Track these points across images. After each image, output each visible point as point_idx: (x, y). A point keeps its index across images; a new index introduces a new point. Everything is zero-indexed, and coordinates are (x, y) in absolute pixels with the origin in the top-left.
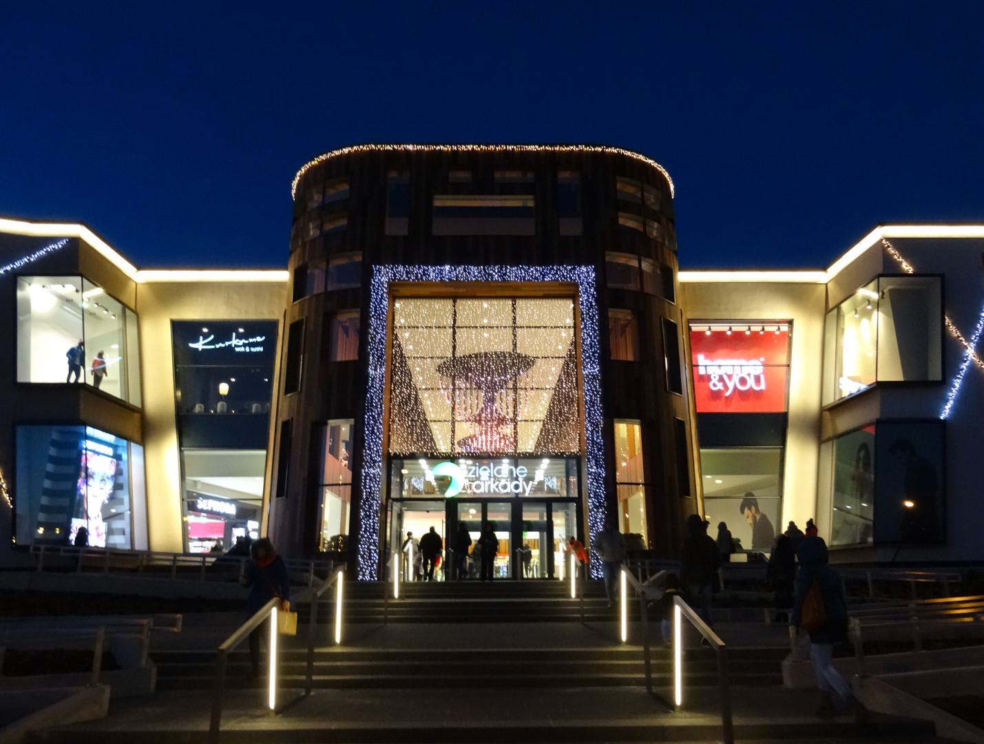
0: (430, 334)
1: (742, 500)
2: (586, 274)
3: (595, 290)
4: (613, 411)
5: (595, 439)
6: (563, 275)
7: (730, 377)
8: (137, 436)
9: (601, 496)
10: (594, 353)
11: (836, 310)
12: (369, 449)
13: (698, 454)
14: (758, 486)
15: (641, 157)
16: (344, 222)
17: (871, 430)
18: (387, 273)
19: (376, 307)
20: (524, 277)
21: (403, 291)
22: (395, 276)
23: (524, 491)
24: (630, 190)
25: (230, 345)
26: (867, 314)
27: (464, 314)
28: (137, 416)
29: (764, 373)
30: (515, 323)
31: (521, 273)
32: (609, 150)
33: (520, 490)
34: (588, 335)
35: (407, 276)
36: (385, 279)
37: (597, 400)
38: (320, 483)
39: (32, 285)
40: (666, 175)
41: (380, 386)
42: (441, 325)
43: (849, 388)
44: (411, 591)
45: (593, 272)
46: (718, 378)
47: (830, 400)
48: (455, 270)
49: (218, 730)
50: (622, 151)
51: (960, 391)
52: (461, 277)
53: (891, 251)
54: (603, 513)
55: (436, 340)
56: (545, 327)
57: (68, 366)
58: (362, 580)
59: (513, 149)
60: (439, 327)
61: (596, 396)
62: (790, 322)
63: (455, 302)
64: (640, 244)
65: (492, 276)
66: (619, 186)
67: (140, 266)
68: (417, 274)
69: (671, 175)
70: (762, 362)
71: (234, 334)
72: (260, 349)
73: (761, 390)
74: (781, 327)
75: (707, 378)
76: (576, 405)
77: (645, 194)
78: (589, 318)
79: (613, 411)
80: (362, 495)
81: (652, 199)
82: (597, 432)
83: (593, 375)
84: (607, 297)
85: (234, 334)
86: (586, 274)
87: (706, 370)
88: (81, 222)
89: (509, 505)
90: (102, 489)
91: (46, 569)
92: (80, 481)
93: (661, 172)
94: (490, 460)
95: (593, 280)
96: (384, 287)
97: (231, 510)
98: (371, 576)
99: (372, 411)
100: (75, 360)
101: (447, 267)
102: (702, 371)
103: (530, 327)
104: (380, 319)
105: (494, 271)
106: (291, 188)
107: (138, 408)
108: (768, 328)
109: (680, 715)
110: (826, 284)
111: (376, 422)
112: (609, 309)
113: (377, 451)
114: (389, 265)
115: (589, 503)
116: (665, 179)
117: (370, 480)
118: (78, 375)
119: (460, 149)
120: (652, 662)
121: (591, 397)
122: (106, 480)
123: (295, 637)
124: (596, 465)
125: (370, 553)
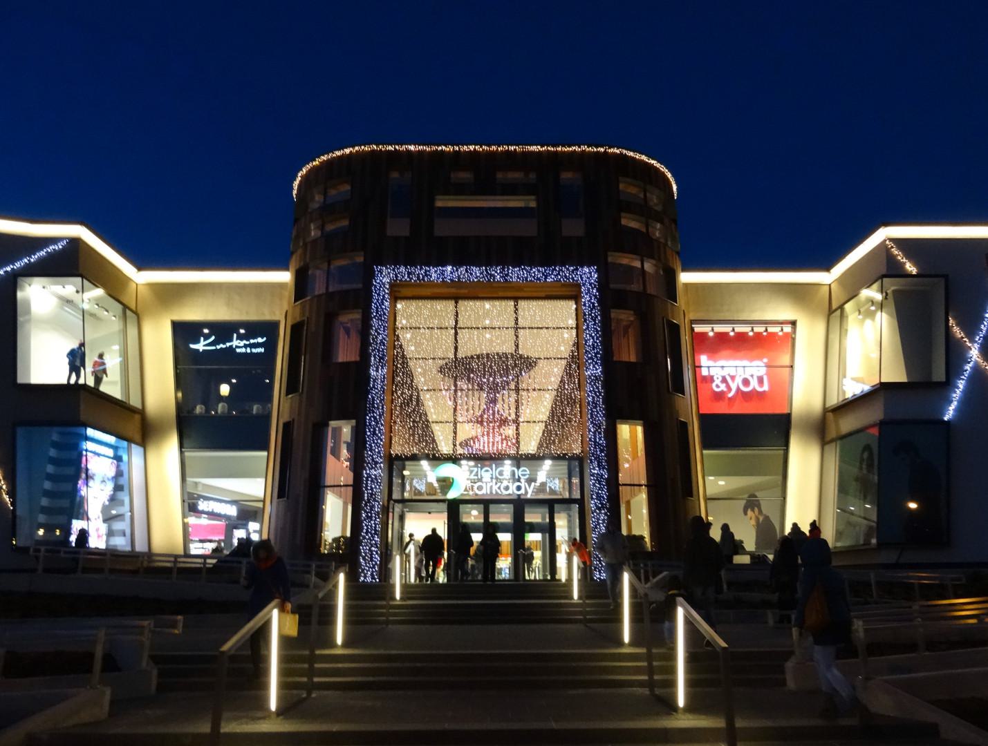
0: (431, 335)
1: (745, 501)
2: (588, 275)
3: (597, 291)
4: (616, 412)
5: (598, 440)
6: (566, 276)
7: (733, 378)
8: (138, 437)
9: (603, 497)
10: (596, 354)
11: (839, 311)
12: (371, 450)
13: (701, 456)
14: (761, 487)
15: (644, 158)
16: (345, 223)
17: (875, 432)
18: (389, 273)
19: (377, 308)
20: (527, 278)
21: (405, 292)
22: (397, 276)
23: (526, 492)
24: (633, 190)
25: (231, 346)
26: (871, 315)
27: (466, 314)
28: (137, 417)
29: (767, 374)
30: (517, 324)
31: (524, 274)
32: (611, 150)
33: (522, 491)
34: (591, 335)
35: (408, 277)
36: (386, 280)
37: (599, 401)
38: (322, 484)
39: (32, 286)
40: (669, 175)
41: (382, 387)
42: (443, 326)
43: (853, 389)
44: (412, 593)
45: (595, 273)
46: (720, 379)
47: (833, 401)
48: (457, 270)
50: (624, 152)
51: (964, 392)
52: (463, 278)
53: (895, 251)
54: (605, 514)
55: (438, 341)
56: (547, 328)
57: (68, 367)
58: (364, 581)
59: (515, 150)
60: (441, 328)
61: (598, 397)
62: (794, 323)
63: (456, 303)
64: (642, 245)
65: (494, 276)
66: (621, 186)
67: (140, 267)
68: (418, 274)
69: (673, 175)
70: (765, 363)
71: (235, 335)
72: (261, 350)
73: (764, 391)
74: (784, 328)
75: (710, 379)
76: (578, 406)
77: (648, 195)
78: (592, 319)
79: (616, 412)
80: (364, 496)
81: (654, 199)
82: (600, 433)
83: (595, 376)
84: (610, 298)
85: (235, 335)
86: (588, 275)
87: (709, 371)
88: (82, 223)
89: (511, 506)
90: (102, 490)
91: (46, 570)
92: (80, 482)
93: (663, 173)
94: (492, 462)
95: (595, 281)
96: (386, 288)
97: (232, 511)
98: (373, 578)
99: (373, 412)
100: (76, 361)
101: (449, 268)
102: (704, 372)
103: (532, 328)
104: (381, 320)
105: (496, 272)
106: (292, 189)
107: (138, 409)
108: (772, 329)
109: (683, 717)
110: (830, 285)
111: (377, 423)
112: (612, 310)
113: (379, 452)
114: (391, 266)
115: (592, 504)
116: (668, 179)
117: (372, 481)
118: (78, 376)
119: (462, 149)
120: (655, 663)
121: (593, 398)
122: (107, 481)
123: (296, 638)
124: (599, 466)
125: (372, 554)
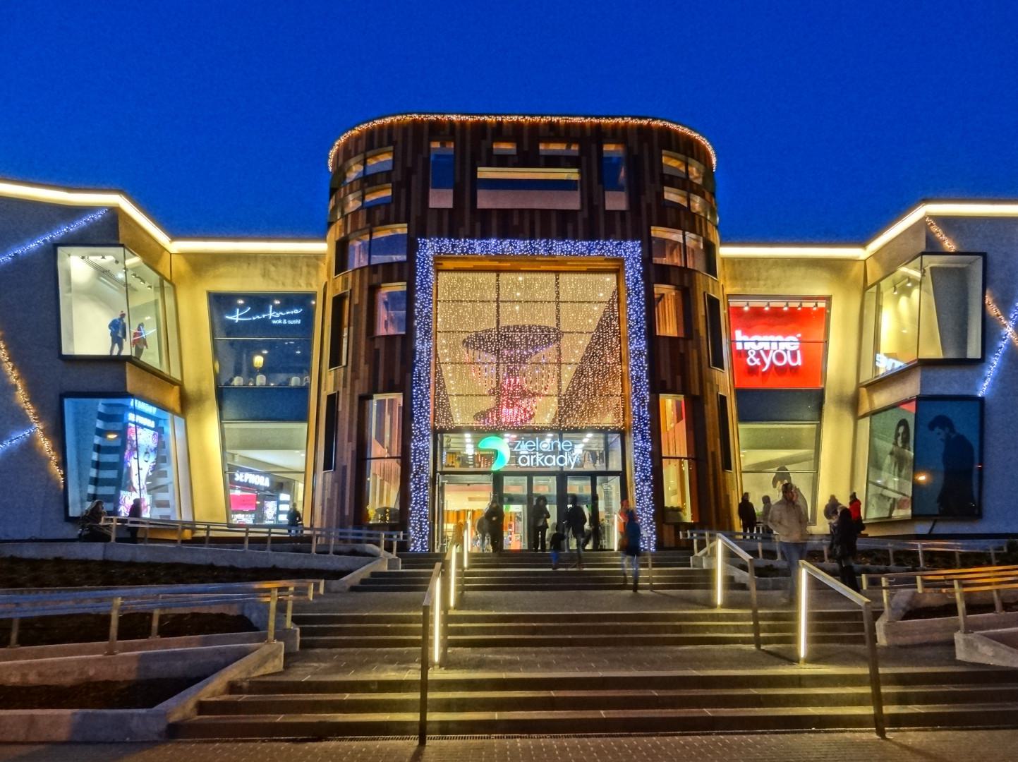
0: (474, 309)
1: (774, 474)
2: (632, 249)
3: (641, 265)
4: (658, 387)
5: (641, 414)
6: (609, 251)
7: (767, 352)
8: (178, 409)
9: (647, 470)
10: (640, 328)
11: (875, 287)
12: (418, 423)
13: (741, 432)
14: (792, 461)
15: (687, 131)
16: (388, 193)
17: (912, 408)
18: (433, 246)
19: (422, 281)
20: (570, 252)
21: (448, 264)
22: (441, 249)
23: (569, 465)
24: (674, 163)
25: (267, 317)
26: (906, 292)
27: (507, 288)
28: (177, 388)
29: (801, 349)
30: (558, 298)
31: (567, 248)
32: (654, 123)
34: (634, 310)
35: (453, 250)
36: (430, 253)
37: (642, 375)
39: (71, 257)
40: (710, 149)
41: (428, 361)
42: (485, 299)
43: (886, 365)
44: (478, 561)
45: (639, 247)
46: (754, 353)
47: (867, 376)
48: (501, 243)
49: (427, 680)
50: (668, 124)
51: (998, 369)
52: (507, 252)
53: (935, 229)
54: (649, 486)
55: (480, 315)
56: (589, 302)
57: (110, 338)
58: (413, 551)
59: (558, 121)
60: (483, 301)
61: (642, 371)
62: (828, 299)
63: (498, 276)
64: (682, 218)
65: (538, 250)
66: (664, 159)
67: (175, 235)
68: (462, 247)
69: (714, 148)
70: (799, 338)
71: (271, 307)
72: (298, 322)
73: (798, 366)
74: (789, 303)
75: (744, 354)
76: (619, 380)
77: (690, 169)
78: (635, 293)
79: (658, 387)
80: (412, 469)
81: (695, 172)
82: (643, 407)
83: (639, 351)
84: (654, 273)
85: (271, 307)
86: (632, 249)
87: (770, 345)
88: (120, 191)
89: (554, 478)
90: (147, 461)
91: (118, 540)
92: (126, 453)
93: (704, 147)
94: (535, 435)
95: (639, 256)
96: (430, 261)
97: (264, 482)
98: (423, 548)
99: (420, 385)
100: (118, 332)
101: (493, 241)
102: (739, 347)
103: (574, 302)
104: (425, 292)
105: (540, 246)
106: (328, 157)
107: (178, 380)
108: (807, 304)
109: (803, 666)
110: (865, 261)
111: (424, 396)
112: (655, 285)
113: (426, 425)
114: (435, 238)
115: (632, 477)
116: (708, 153)
117: (420, 453)
118: (121, 347)
119: (504, 120)
120: (760, 623)
121: (637, 372)
122: (150, 452)
124: (643, 439)
125: (421, 525)
